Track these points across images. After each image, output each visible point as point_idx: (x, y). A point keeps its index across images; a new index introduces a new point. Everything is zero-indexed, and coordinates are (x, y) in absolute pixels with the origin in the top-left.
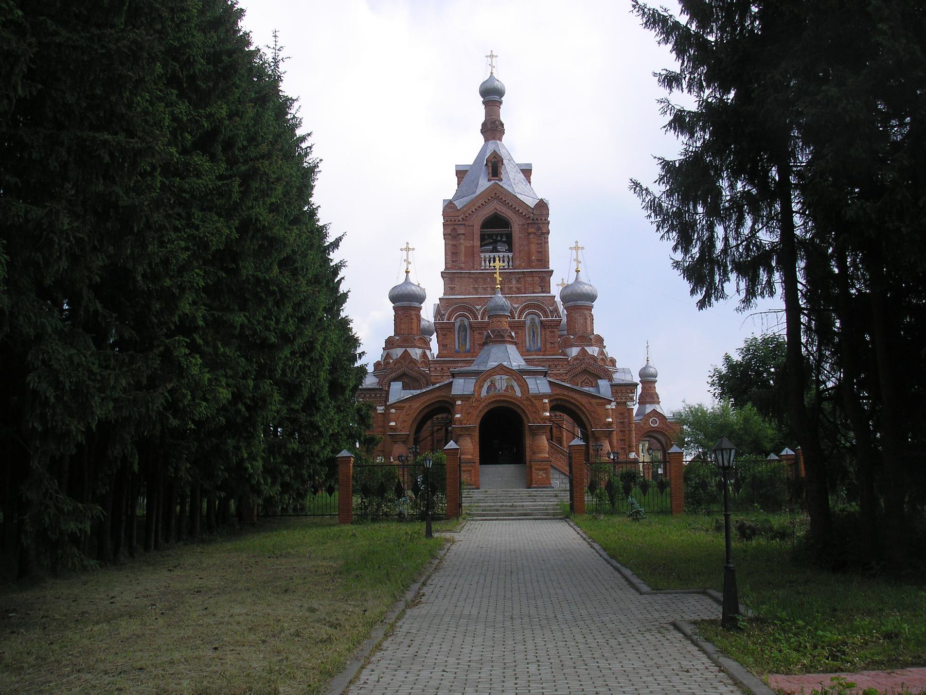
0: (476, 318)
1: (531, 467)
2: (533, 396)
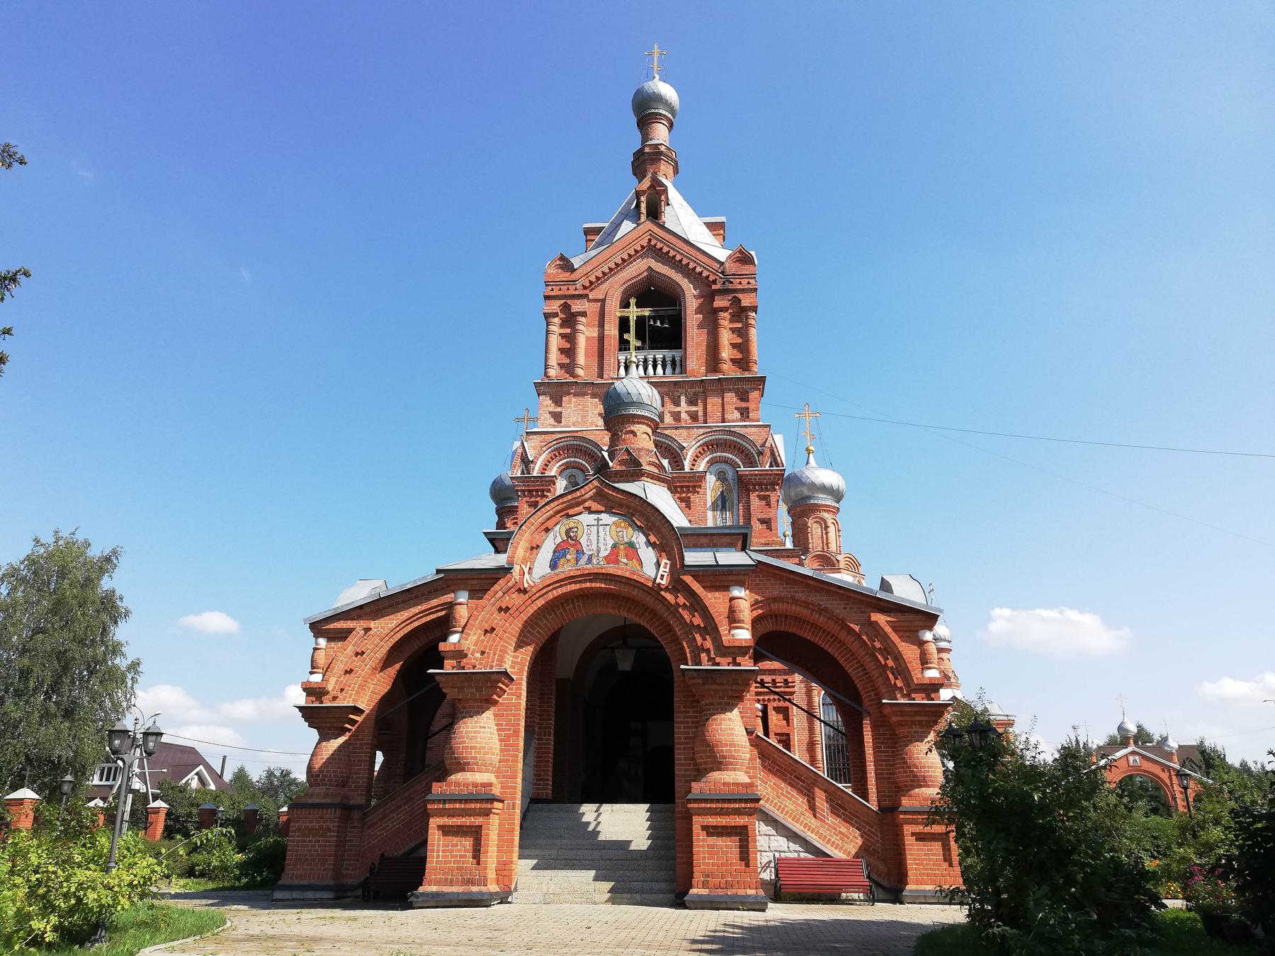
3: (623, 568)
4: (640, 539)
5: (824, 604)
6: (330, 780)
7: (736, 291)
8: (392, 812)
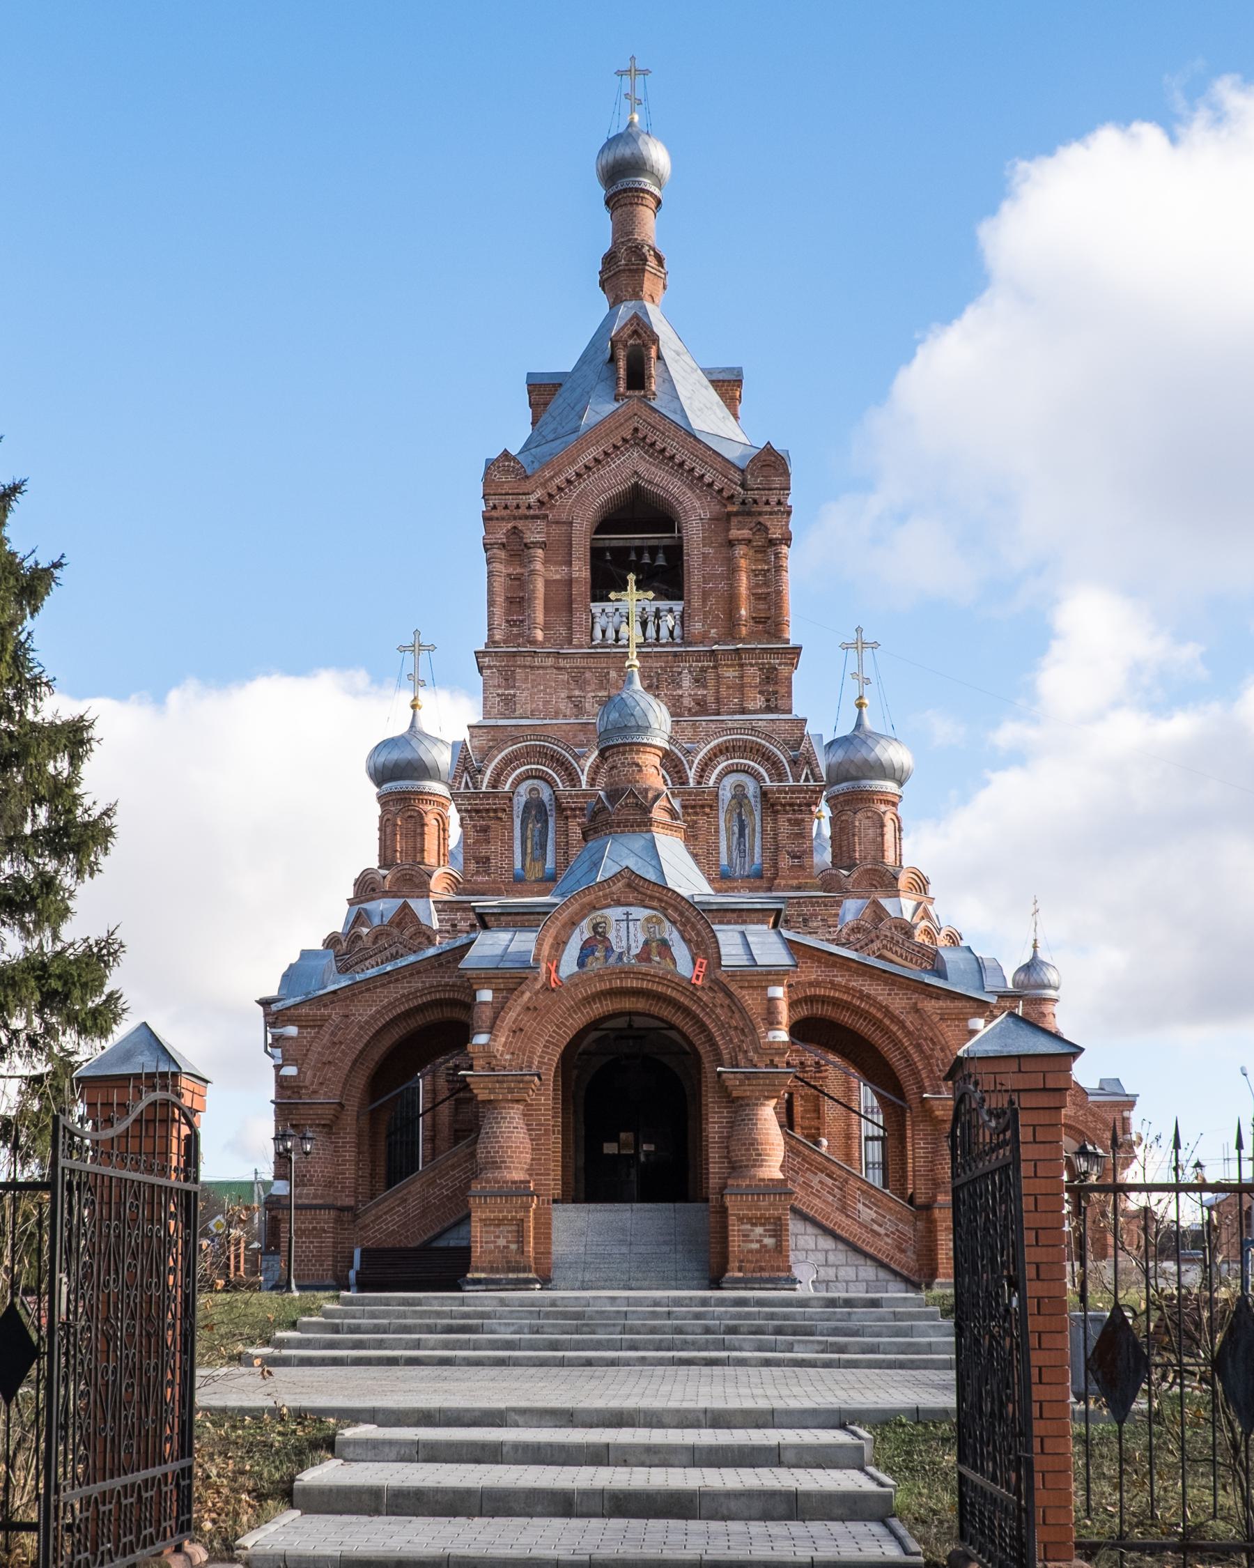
0: (573, 778)
1: (723, 1211)
2: (732, 976)
5: (865, 989)
7: (760, 514)
8: (385, 1213)
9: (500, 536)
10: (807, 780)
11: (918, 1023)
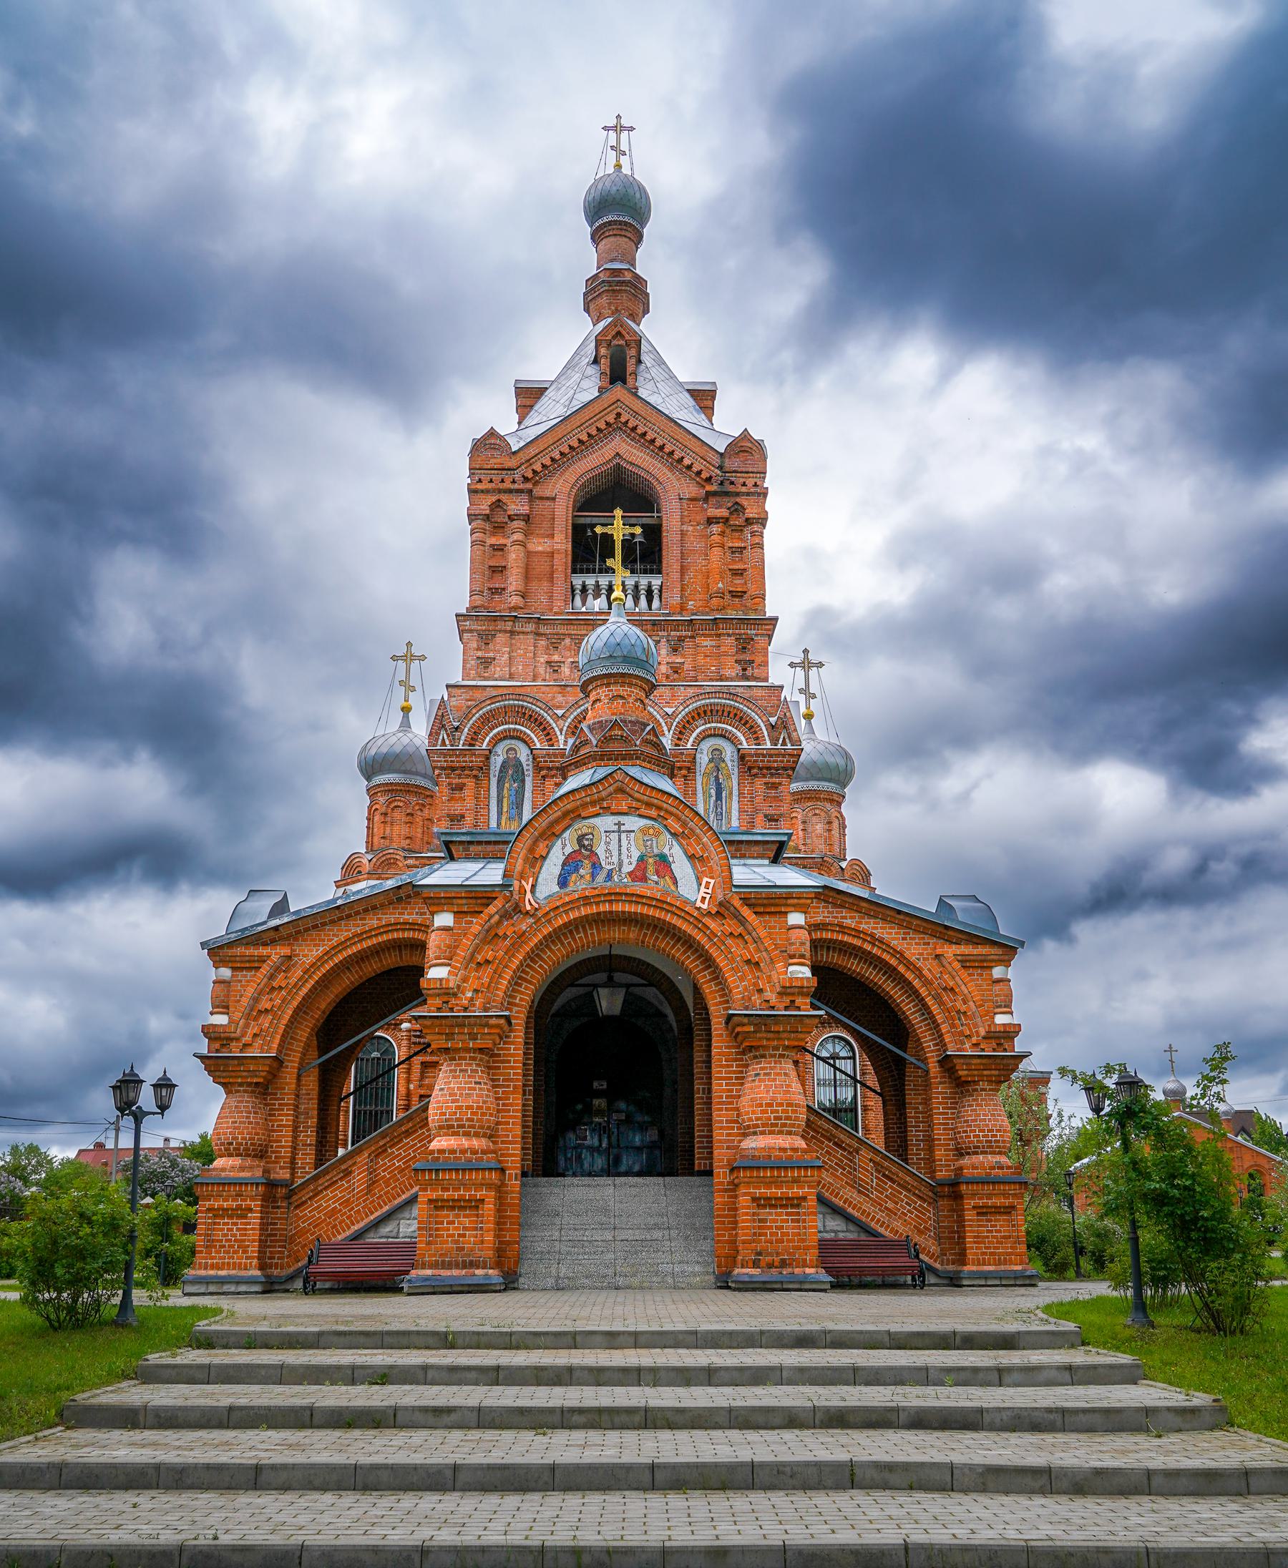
0: (549, 736)
3: (654, 885)
4: (676, 854)
6: (246, 1149)
7: (738, 494)
8: (326, 1188)
9: (484, 508)
10: (784, 743)
11: (937, 970)
